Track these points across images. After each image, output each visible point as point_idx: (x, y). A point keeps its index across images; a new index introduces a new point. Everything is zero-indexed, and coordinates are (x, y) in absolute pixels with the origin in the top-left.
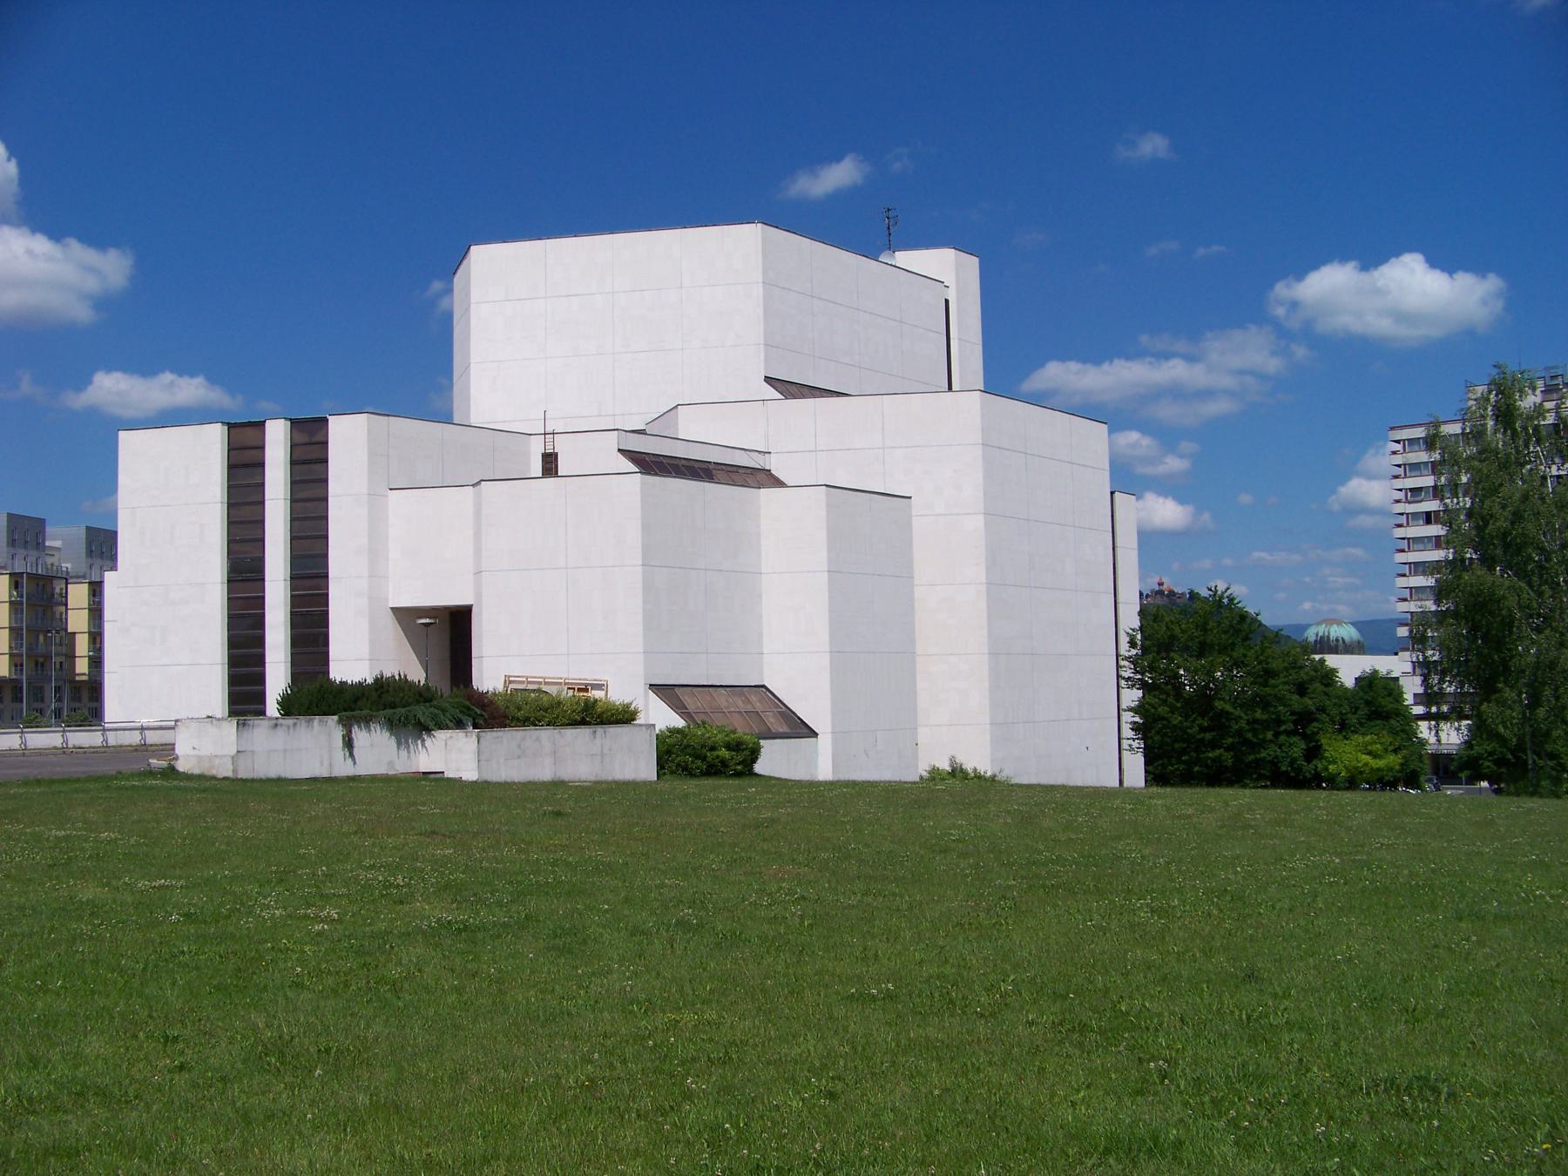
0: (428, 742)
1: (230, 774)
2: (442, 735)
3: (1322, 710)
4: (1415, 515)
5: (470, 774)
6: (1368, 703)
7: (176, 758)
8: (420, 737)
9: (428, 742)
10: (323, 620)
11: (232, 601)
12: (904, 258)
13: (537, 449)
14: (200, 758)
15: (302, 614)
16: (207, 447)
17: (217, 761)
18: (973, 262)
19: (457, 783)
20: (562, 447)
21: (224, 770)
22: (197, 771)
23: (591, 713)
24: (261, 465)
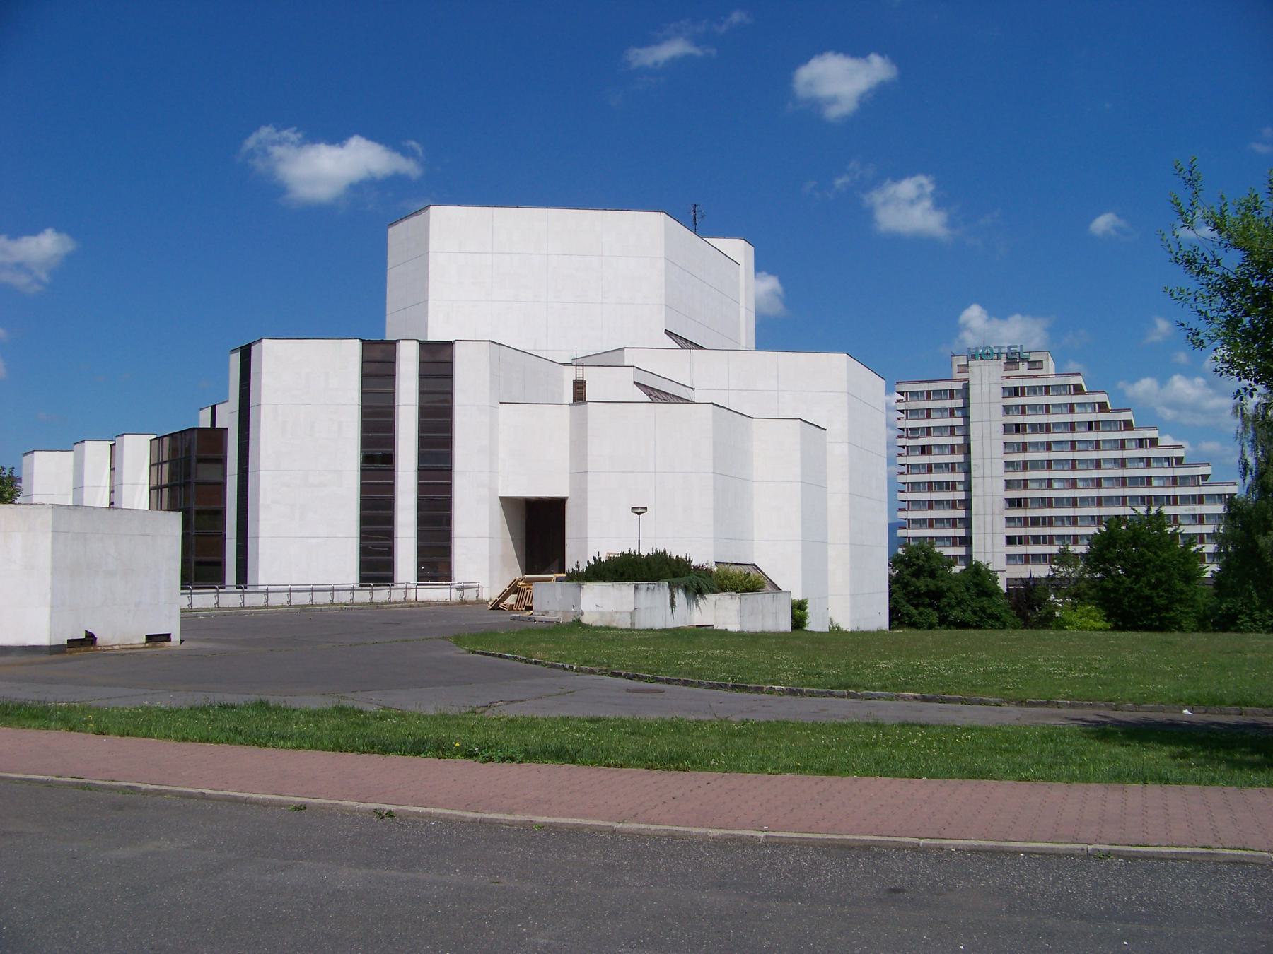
0: (701, 602)
1: (628, 626)
2: (711, 597)
3: (950, 589)
4: (913, 448)
5: (734, 627)
6: (976, 585)
7: (582, 614)
8: (695, 598)
9: (701, 602)
10: (447, 504)
11: (364, 488)
12: (716, 242)
13: (569, 375)
14: (602, 614)
15: (428, 499)
16: (344, 358)
17: (617, 616)
18: (752, 249)
19: (724, 633)
20: (593, 377)
21: (625, 623)
22: (599, 624)
23: (746, 582)
24: (392, 376)
